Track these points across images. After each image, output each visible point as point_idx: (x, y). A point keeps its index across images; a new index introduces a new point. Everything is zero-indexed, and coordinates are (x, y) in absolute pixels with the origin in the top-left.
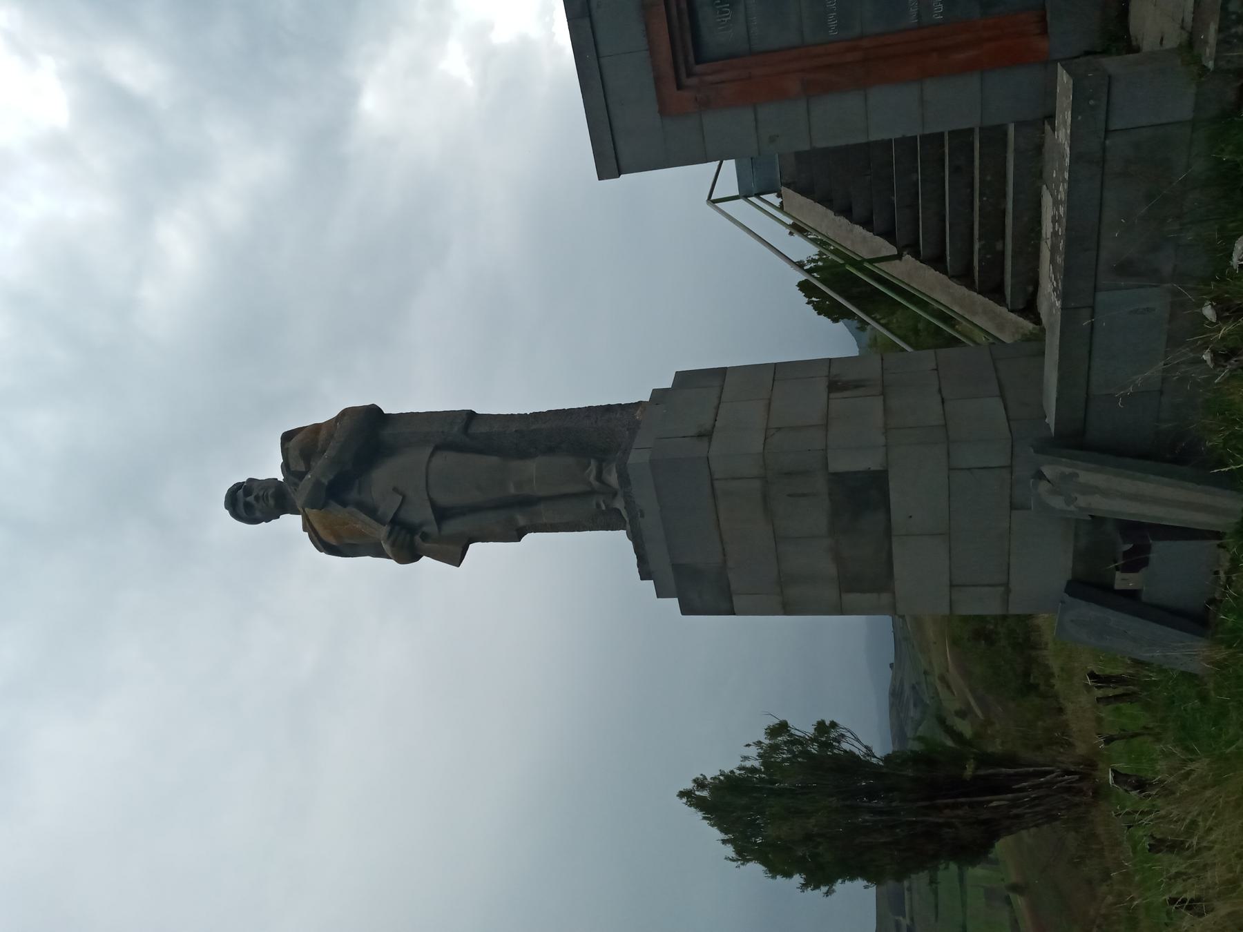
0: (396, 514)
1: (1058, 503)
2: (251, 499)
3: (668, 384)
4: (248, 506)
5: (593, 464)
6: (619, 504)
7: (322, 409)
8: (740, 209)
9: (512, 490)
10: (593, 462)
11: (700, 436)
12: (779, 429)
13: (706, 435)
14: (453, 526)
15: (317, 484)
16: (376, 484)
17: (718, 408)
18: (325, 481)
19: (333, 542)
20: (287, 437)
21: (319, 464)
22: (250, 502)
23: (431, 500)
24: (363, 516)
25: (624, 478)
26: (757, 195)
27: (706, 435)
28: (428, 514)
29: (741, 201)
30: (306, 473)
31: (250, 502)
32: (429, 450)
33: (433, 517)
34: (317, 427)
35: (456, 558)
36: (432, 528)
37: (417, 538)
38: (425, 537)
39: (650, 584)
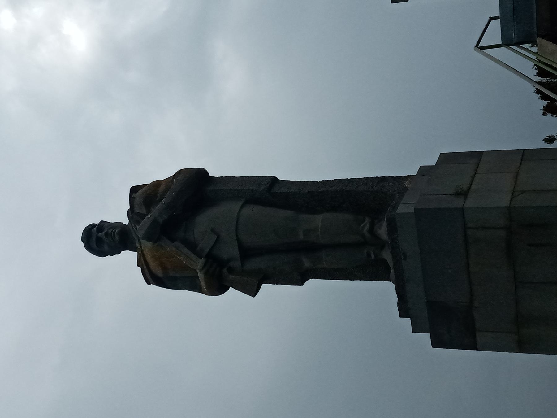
0: (211, 250)
2: (101, 234)
3: (432, 162)
4: (99, 241)
5: (367, 220)
6: (387, 255)
7: (160, 169)
8: (503, 53)
9: (301, 237)
10: (367, 220)
11: (457, 194)
12: (523, 192)
13: (463, 194)
14: (254, 264)
15: (154, 221)
17: (473, 177)
18: (161, 220)
19: (159, 272)
20: (134, 190)
21: (156, 210)
22: (101, 240)
23: (238, 239)
24: (186, 250)
25: (392, 229)
26: (518, 44)
27: (463, 194)
28: (236, 253)
29: (503, 48)
30: (147, 215)
31: (101, 240)
32: (240, 204)
33: (238, 256)
34: (157, 184)
35: (253, 291)
36: (237, 264)
37: (225, 270)
38: (231, 271)
39: (407, 321)
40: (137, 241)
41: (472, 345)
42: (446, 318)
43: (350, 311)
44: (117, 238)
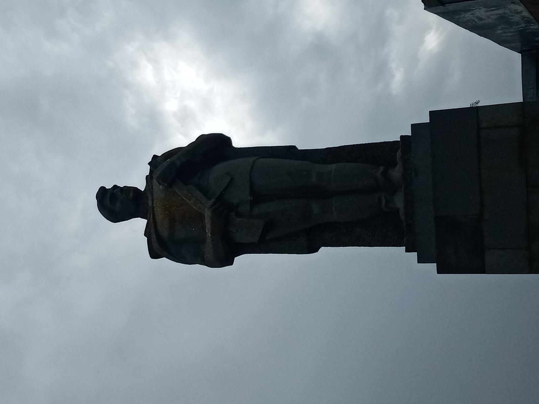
31: (115, 203)
38: (239, 215)
40: (150, 198)
41: (481, 269)
42: (455, 249)
43: (363, 281)
44: (131, 194)
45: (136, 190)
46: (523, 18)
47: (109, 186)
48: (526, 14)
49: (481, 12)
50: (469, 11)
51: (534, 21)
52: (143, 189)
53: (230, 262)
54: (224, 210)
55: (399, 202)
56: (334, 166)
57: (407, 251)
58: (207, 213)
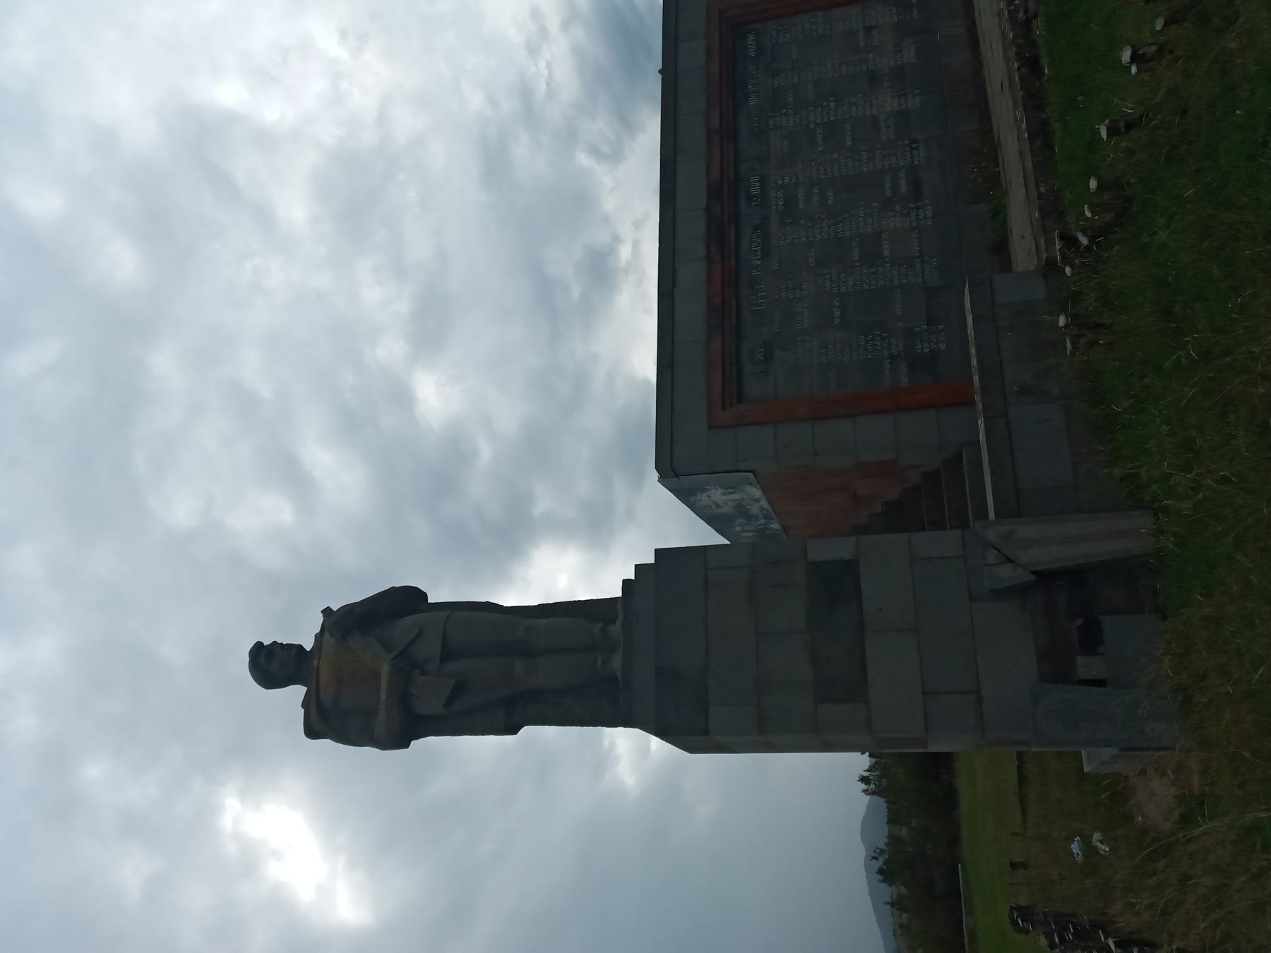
1: (1006, 571)
16: (390, 672)
31: (272, 664)
38: (424, 673)
45: (300, 647)
46: (762, 509)
47: (267, 642)
48: (764, 503)
49: (717, 495)
50: (704, 490)
51: (773, 515)
52: (308, 649)
53: (407, 745)
54: (407, 664)
55: (617, 661)
56: (545, 621)
57: (625, 582)
58: (385, 669)
